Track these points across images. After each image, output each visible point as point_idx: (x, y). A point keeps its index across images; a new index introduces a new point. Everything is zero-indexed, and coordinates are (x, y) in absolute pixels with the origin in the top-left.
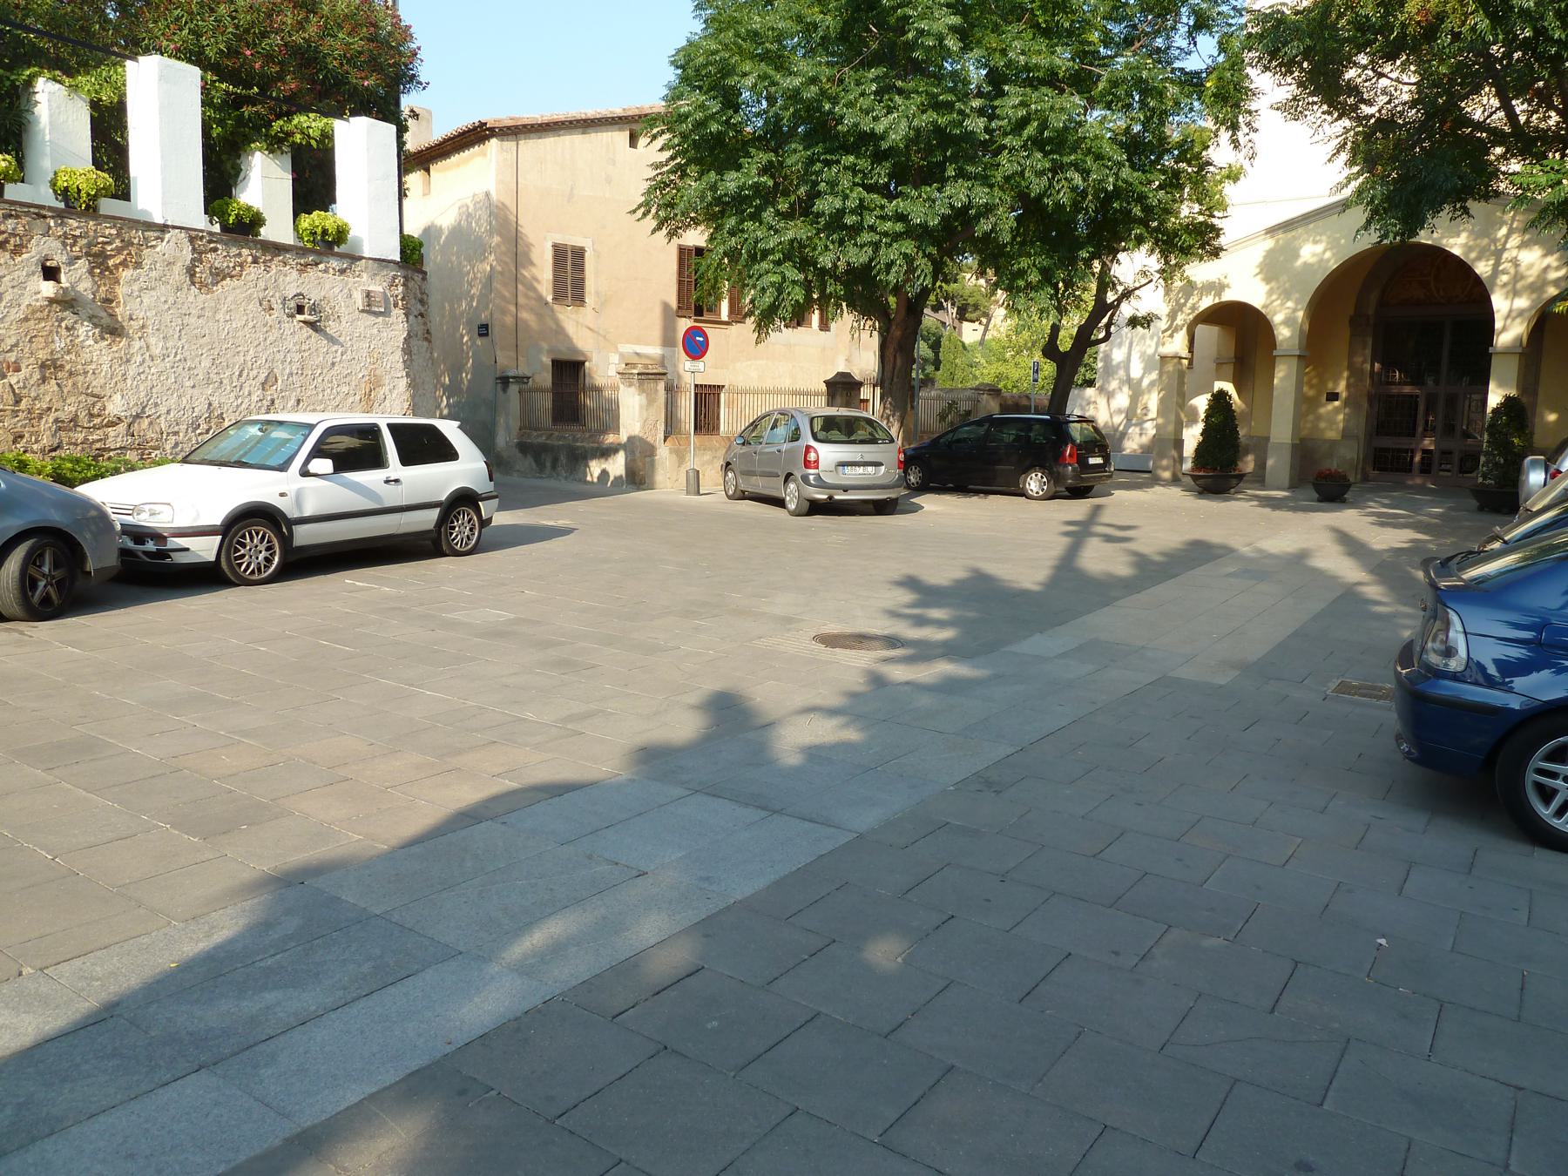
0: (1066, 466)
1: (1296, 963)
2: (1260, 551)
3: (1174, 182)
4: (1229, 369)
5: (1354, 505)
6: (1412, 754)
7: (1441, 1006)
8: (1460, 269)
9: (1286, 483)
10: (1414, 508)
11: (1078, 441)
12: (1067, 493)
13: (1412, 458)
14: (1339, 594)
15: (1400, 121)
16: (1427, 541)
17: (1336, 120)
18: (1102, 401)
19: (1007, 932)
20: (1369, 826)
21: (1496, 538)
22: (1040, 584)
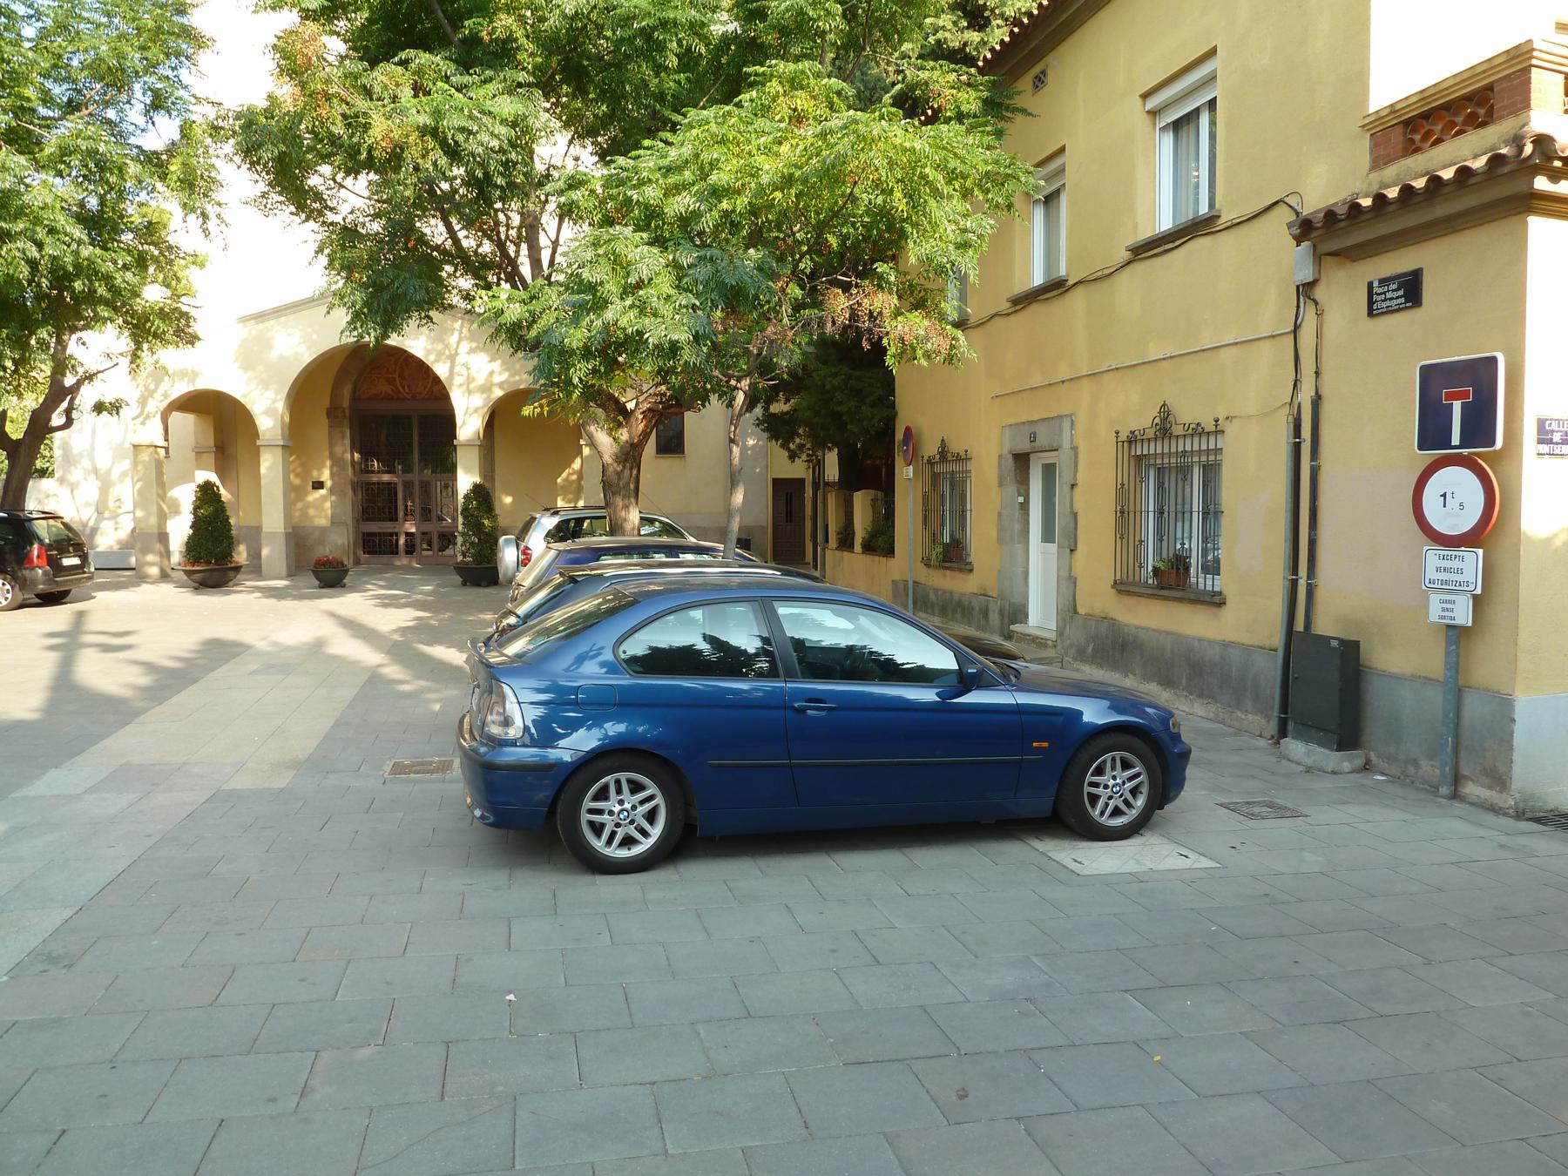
0: (33, 569)
1: (447, 1044)
2: (276, 644)
3: (141, 262)
4: (210, 458)
5: (355, 589)
6: (488, 818)
7: (575, 1037)
8: (421, 370)
9: (284, 573)
10: (409, 588)
11: (47, 541)
12: (37, 600)
13: (397, 540)
14: (366, 678)
15: (364, 232)
16: (428, 618)
17: (303, 222)
18: (64, 491)
19: (141, 1123)
20: (463, 894)
21: (511, 613)
22: (37, 710)
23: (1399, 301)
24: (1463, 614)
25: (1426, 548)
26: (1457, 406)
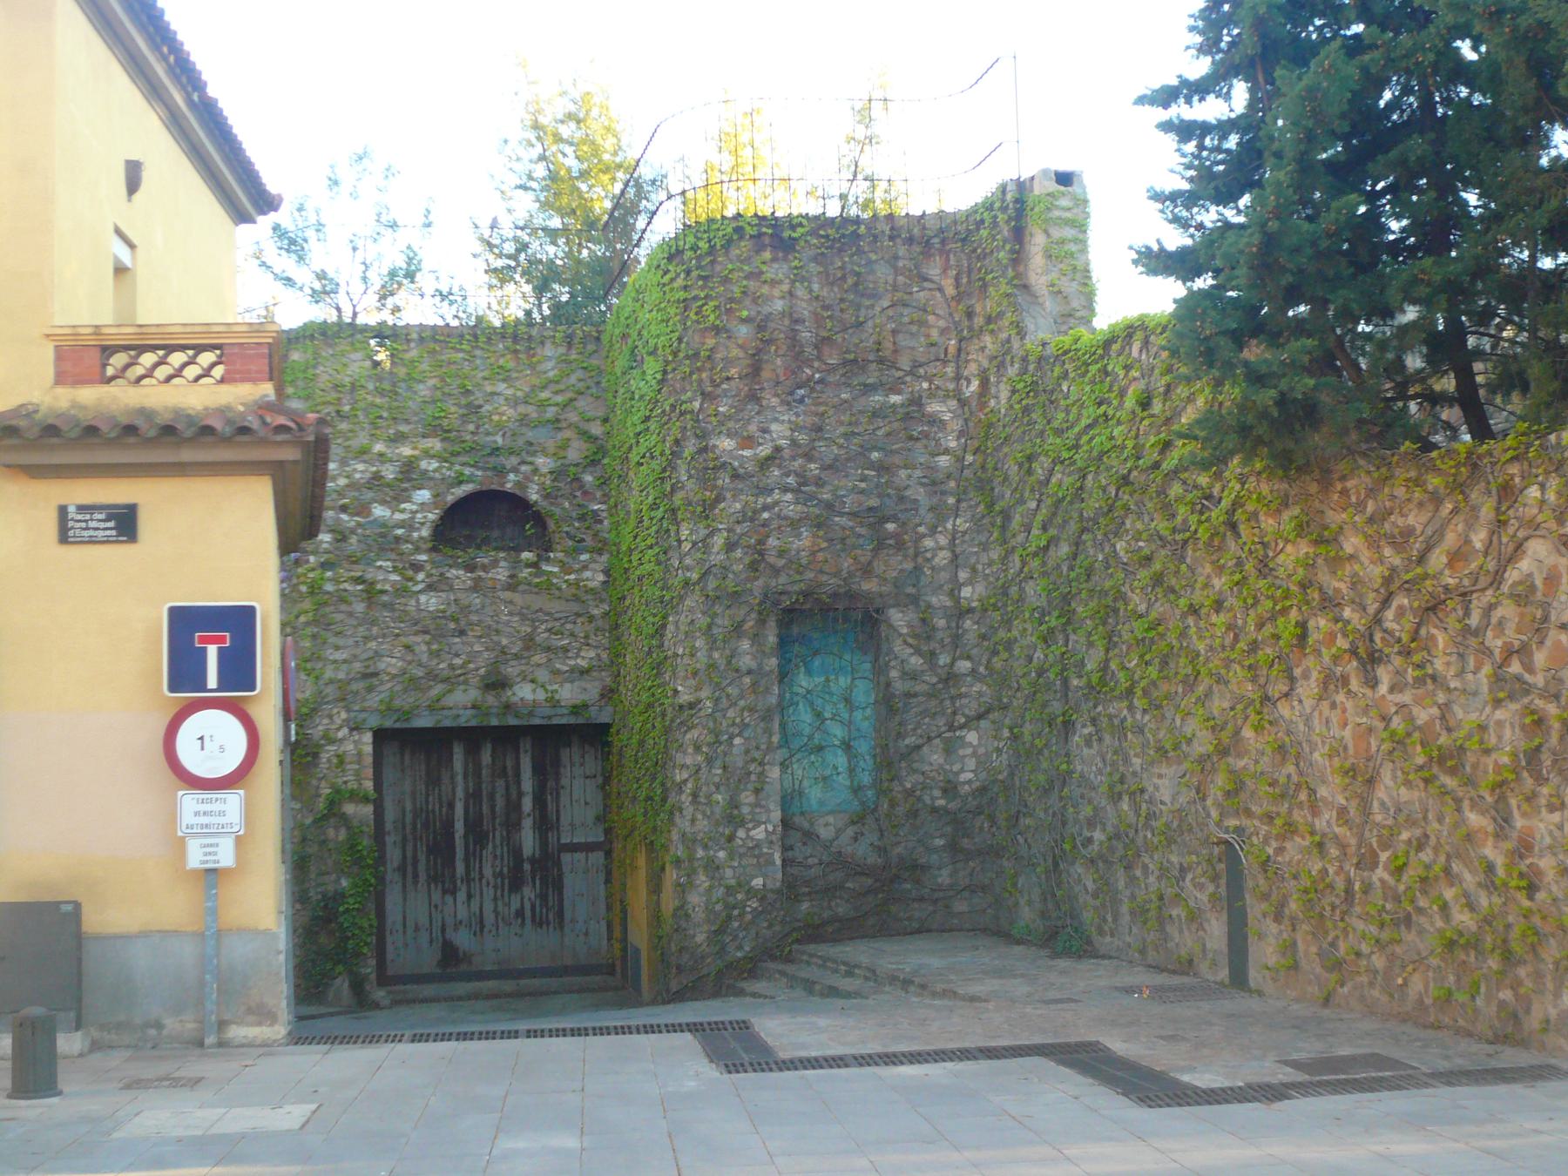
12: (1302, 1077)
23: (108, 533)
24: (226, 856)
25: (181, 793)
26: (212, 651)
